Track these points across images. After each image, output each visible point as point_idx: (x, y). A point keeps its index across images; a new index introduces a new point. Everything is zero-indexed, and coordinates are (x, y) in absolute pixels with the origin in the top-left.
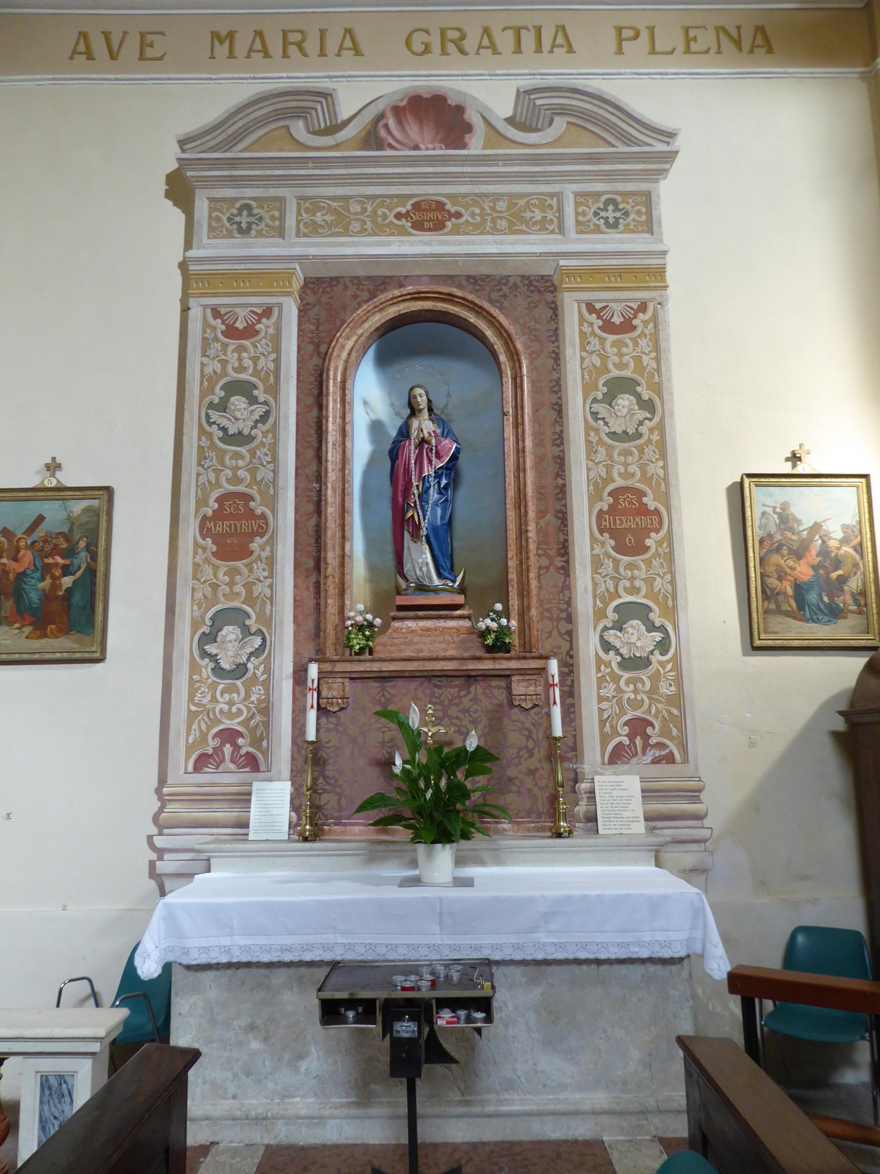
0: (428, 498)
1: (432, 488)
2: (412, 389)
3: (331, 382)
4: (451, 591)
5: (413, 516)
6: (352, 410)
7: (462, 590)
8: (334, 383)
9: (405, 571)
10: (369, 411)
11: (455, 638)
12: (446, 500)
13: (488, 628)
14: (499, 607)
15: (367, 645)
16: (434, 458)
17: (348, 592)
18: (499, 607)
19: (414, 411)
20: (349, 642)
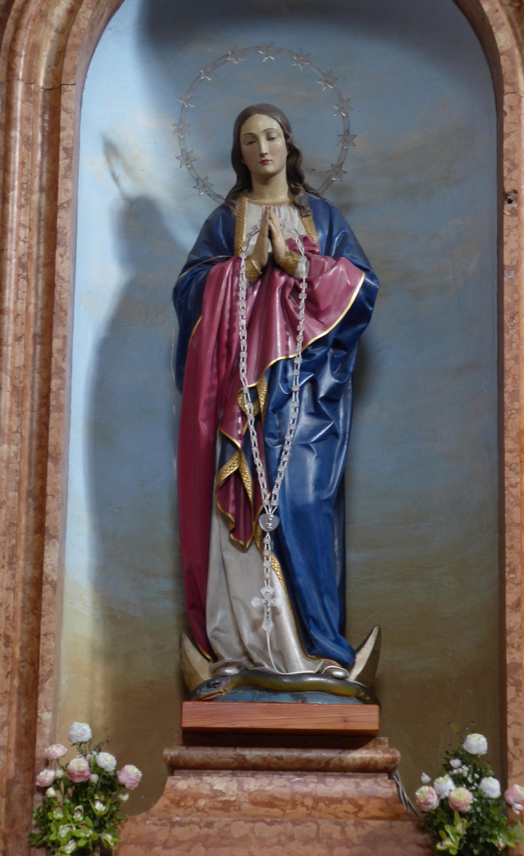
0: (283, 425)
1: (295, 397)
2: (244, 117)
3: (20, 89)
4: (337, 691)
5: (238, 474)
6: (73, 170)
7: (369, 690)
8: (28, 92)
9: (210, 629)
10: (119, 171)
11: (351, 830)
12: (333, 433)
13: (445, 803)
14: (477, 743)
15: (98, 843)
16: (302, 315)
17: (47, 686)
18: (477, 743)
19: (248, 179)
20: (47, 831)
